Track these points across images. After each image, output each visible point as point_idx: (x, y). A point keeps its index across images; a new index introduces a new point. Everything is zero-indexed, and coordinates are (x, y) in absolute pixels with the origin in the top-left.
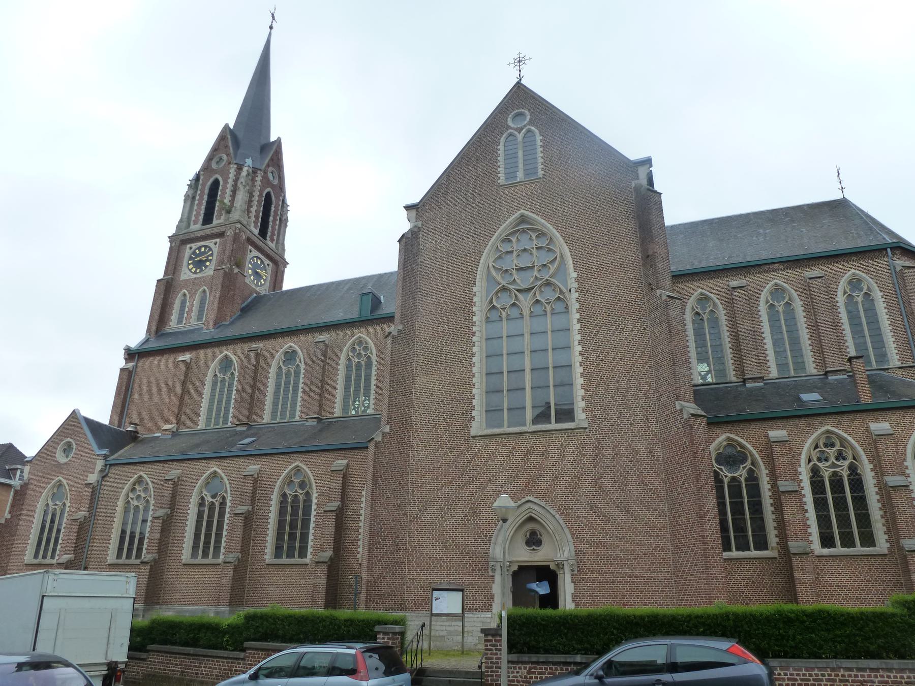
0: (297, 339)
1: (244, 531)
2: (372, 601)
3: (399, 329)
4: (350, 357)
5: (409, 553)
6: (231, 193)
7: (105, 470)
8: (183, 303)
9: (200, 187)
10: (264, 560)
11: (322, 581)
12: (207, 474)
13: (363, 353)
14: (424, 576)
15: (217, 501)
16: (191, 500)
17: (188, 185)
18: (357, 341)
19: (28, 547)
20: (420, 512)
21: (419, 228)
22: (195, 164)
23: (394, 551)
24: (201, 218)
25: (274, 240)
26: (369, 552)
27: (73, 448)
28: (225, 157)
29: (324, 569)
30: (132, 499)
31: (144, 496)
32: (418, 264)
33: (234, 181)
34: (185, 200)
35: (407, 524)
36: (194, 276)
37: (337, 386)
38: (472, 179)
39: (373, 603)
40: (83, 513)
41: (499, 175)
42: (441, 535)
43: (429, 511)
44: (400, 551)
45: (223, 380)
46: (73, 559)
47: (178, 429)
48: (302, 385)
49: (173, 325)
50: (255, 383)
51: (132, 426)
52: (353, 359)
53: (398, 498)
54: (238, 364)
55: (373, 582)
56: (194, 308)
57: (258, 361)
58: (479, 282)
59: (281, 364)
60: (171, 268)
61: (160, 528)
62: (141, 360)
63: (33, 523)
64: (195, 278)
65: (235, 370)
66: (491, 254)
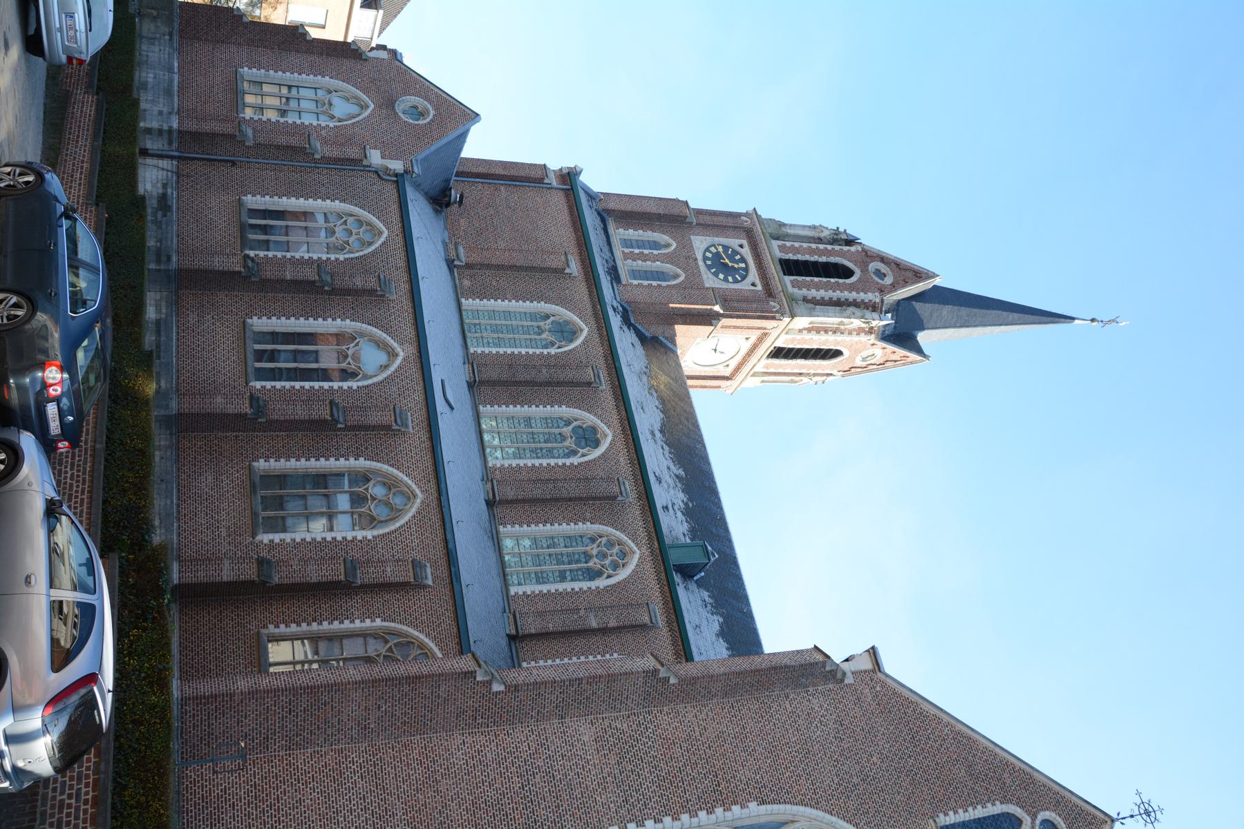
0: (620, 444)
1: (303, 422)
2: (197, 707)
3: (671, 679)
4: (600, 540)
5: (285, 757)
6: (835, 299)
7: (389, 175)
8: (655, 245)
9: (837, 248)
10: (256, 459)
11: (227, 573)
12: (392, 341)
13: (607, 562)
14: (244, 793)
15: (349, 364)
16: (348, 321)
17: (838, 228)
18: (627, 548)
19: (263, 71)
20: (357, 767)
21: (842, 681)
22: (872, 238)
23: (287, 731)
24: (791, 256)
25: (767, 368)
26: (282, 690)
27: (418, 120)
28: (888, 280)
29: (249, 572)
30: (345, 222)
31: (350, 242)
32: (782, 690)
33: (855, 300)
34: (814, 227)
35: (335, 744)
36: (699, 257)
37: (548, 525)
38: (937, 764)
39: (194, 709)
40: (320, 149)
41: (951, 813)
42: (320, 814)
43: (361, 783)
44: (286, 741)
45: (540, 331)
46: (247, 144)
47: (458, 267)
48: (545, 465)
49: (619, 233)
50: (541, 384)
51: (458, 196)
52: (595, 545)
53: (378, 724)
54: (570, 351)
55: (231, 705)
56: (649, 263)
57: (578, 384)
58: (766, 810)
59: (575, 423)
60: (708, 219)
61: (300, 278)
62: (561, 194)
63: (300, 74)
64: (696, 259)
65: (559, 347)
66: (815, 822)
